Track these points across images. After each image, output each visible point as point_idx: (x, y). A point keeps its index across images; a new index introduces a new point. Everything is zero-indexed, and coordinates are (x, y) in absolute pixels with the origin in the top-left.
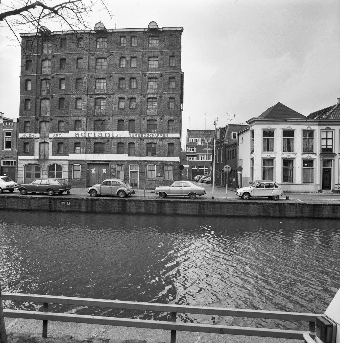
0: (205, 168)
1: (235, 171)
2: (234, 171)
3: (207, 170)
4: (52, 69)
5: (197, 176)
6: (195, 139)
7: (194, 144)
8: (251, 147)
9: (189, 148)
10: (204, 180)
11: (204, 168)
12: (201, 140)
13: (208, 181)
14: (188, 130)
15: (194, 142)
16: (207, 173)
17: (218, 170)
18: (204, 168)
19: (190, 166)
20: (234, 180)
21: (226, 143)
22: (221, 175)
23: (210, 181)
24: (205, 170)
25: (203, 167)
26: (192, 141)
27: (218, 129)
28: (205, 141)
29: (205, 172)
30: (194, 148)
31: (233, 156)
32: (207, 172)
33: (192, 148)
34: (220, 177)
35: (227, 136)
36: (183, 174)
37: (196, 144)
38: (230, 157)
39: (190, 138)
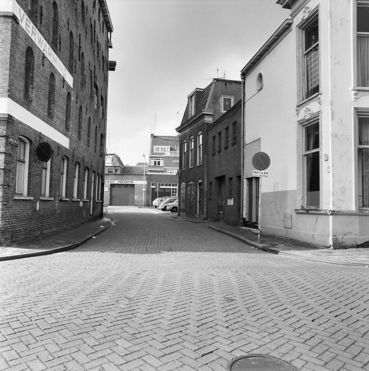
0: (173, 185)
1: (235, 178)
2: (231, 179)
3: (176, 189)
4: (179, 198)
5: (157, 199)
6: (162, 148)
7: (160, 154)
8: (299, 82)
9: (153, 161)
10: (166, 206)
11: (171, 187)
12: (171, 149)
13: (174, 208)
14: (152, 135)
15: (160, 151)
16: (175, 195)
17: (191, 183)
18: (171, 187)
19: (148, 184)
20: (231, 202)
21: (209, 120)
22: (196, 194)
23: (176, 208)
24: (173, 189)
25: (170, 185)
26: (158, 150)
27: (191, 97)
28: (176, 150)
29: (173, 192)
30: (161, 161)
31: (227, 142)
32: (176, 192)
33: (157, 161)
34: (195, 199)
35: (211, 105)
36: (136, 197)
37: (164, 154)
38: (220, 147)
39: (154, 147)
